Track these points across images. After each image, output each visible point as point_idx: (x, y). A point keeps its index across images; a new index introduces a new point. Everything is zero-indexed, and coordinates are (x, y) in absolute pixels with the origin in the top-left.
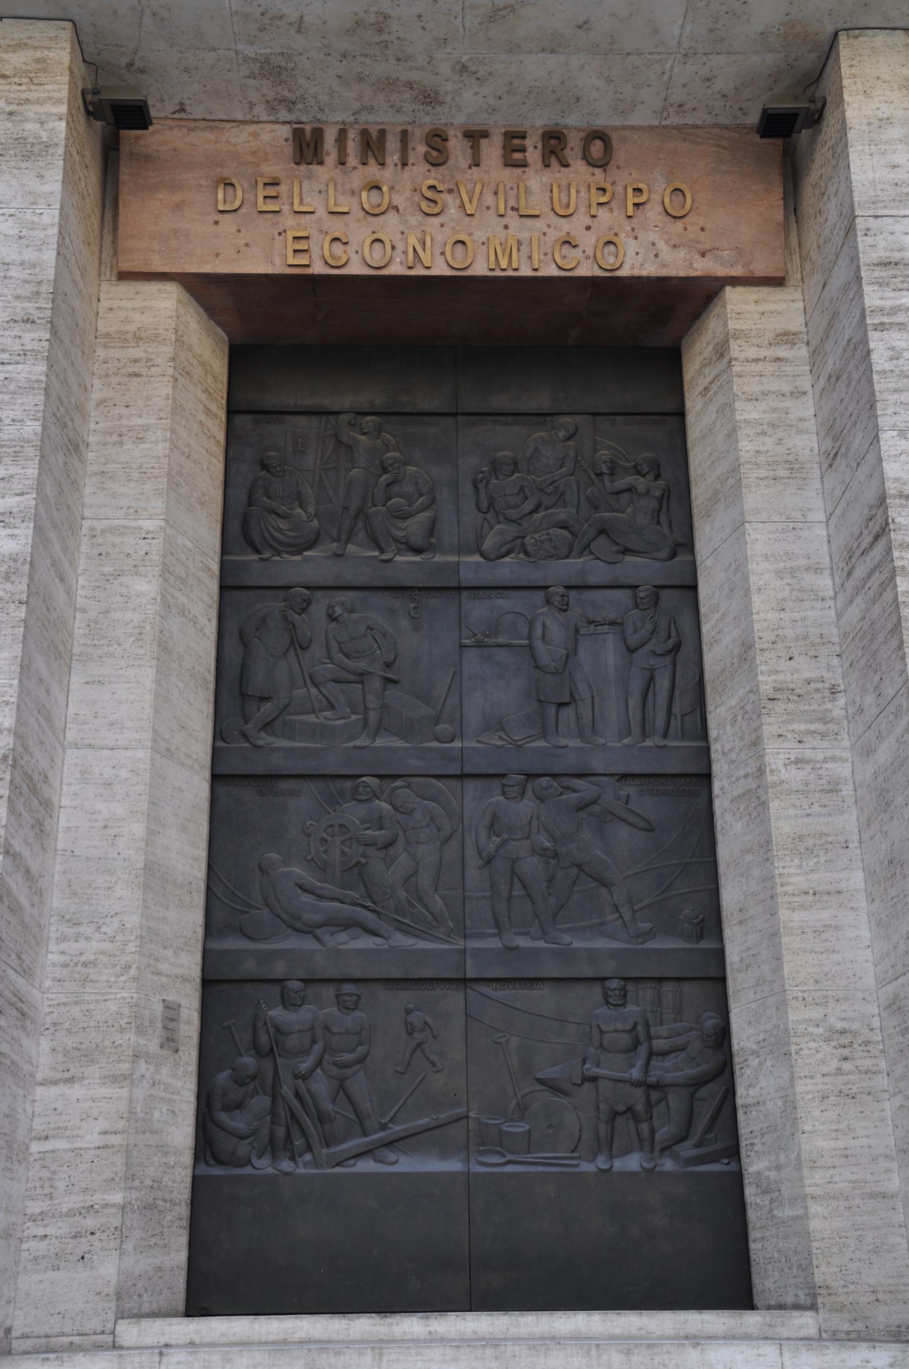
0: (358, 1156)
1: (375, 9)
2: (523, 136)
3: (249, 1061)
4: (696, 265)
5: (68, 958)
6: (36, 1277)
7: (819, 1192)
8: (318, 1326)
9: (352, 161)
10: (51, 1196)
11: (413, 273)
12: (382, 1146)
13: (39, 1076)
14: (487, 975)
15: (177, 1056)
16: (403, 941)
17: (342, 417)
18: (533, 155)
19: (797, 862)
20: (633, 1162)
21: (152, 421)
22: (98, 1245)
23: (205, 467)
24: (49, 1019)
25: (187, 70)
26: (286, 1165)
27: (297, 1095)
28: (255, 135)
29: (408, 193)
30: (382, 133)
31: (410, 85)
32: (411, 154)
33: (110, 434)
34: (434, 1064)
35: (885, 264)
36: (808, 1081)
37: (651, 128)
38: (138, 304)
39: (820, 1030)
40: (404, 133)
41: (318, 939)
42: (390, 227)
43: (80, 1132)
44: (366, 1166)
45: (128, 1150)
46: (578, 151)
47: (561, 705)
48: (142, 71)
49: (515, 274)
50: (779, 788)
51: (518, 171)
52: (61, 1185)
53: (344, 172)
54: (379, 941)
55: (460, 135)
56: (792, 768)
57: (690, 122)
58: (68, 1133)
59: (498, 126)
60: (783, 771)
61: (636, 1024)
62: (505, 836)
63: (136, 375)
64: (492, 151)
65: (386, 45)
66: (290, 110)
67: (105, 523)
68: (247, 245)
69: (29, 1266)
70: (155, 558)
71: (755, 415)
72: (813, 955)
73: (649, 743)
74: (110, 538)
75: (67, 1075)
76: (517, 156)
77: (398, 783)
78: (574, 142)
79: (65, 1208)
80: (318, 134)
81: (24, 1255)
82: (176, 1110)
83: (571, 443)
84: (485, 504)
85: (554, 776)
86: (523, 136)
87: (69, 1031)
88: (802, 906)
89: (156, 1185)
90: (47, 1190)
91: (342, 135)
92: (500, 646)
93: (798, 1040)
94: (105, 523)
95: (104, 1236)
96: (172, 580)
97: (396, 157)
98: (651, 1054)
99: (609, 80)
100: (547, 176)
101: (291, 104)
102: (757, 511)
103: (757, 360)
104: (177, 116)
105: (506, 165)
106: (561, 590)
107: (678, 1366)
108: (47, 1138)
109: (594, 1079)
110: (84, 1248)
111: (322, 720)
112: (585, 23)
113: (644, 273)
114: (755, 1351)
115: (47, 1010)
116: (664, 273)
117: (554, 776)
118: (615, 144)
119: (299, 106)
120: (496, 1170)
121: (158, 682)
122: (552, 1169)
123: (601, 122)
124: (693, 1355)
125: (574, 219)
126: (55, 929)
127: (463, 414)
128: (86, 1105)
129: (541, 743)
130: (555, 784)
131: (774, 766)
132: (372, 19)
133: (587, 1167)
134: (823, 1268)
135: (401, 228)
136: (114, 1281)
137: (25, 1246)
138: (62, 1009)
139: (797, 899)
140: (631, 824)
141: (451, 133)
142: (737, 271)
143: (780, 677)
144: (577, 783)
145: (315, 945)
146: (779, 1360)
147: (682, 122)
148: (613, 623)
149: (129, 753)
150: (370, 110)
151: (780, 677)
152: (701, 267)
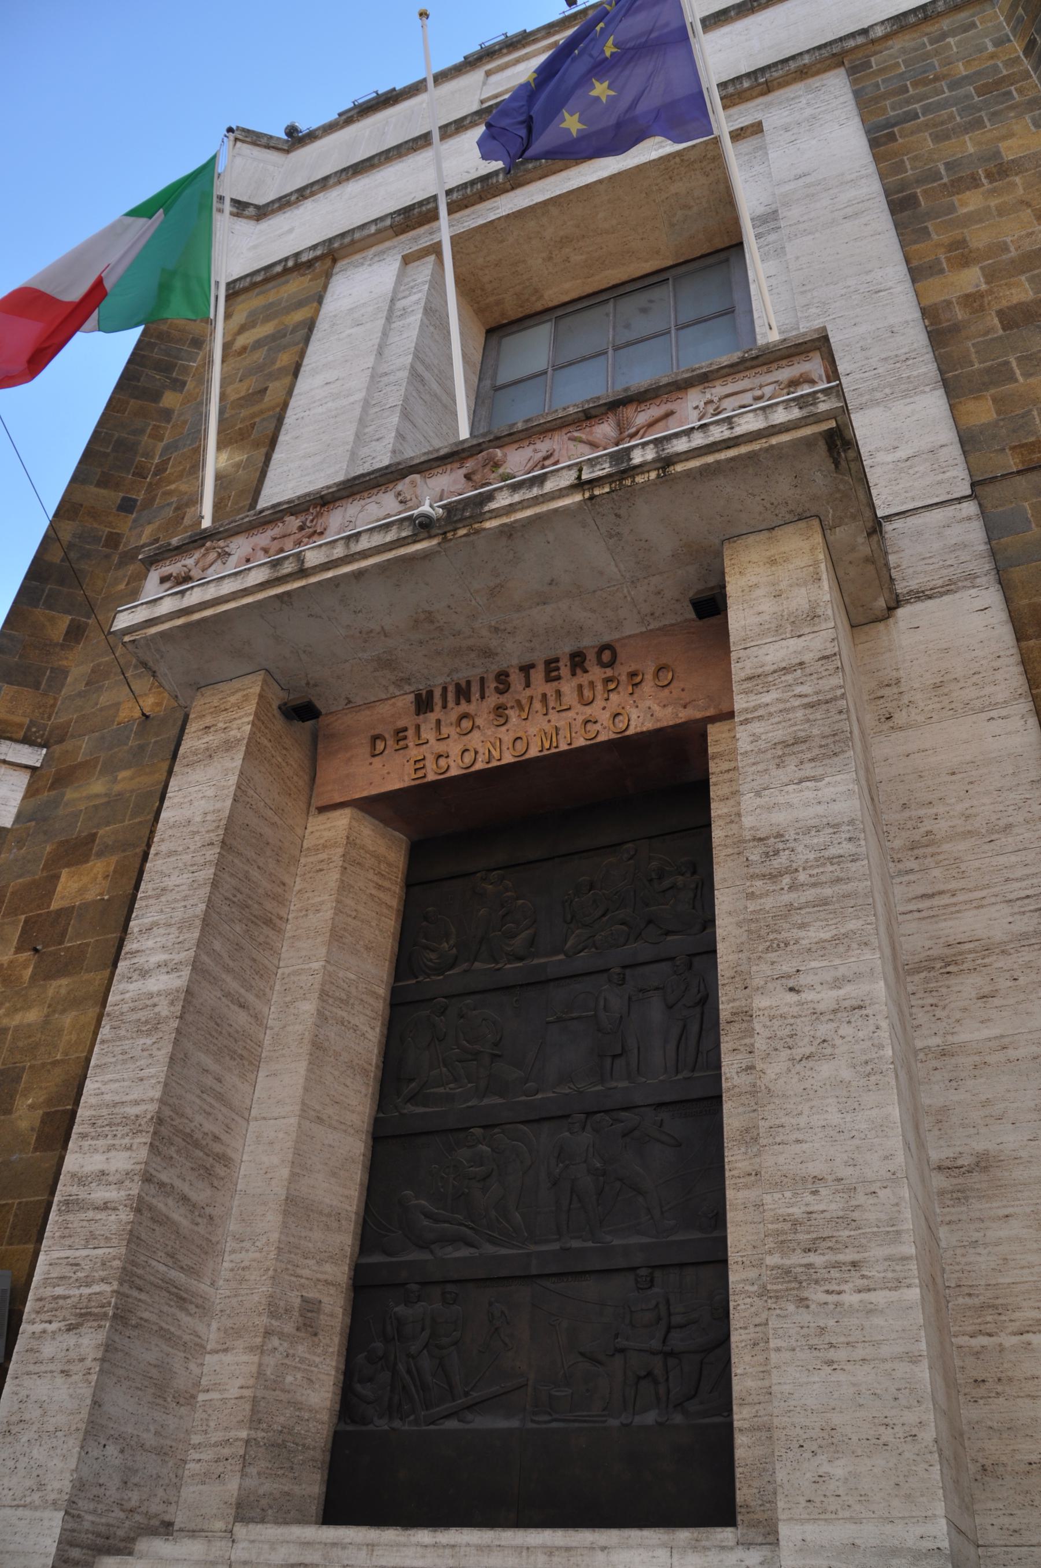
0: (447, 1417)
1: (420, 610)
2: (557, 660)
3: (378, 1345)
4: (680, 715)
5: (234, 1265)
6: (192, 1489)
7: (746, 1425)
8: (360, 1534)
9: (451, 704)
10: (206, 1432)
11: (490, 766)
12: (464, 1409)
13: (209, 1348)
14: (547, 1271)
15: (316, 1339)
16: (490, 1249)
17: (478, 875)
18: (565, 671)
19: (743, 1150)
20: (650, 1418)
21: (326, 897)
22: (229, 1468)
23: (374, 924)
24: (219, 1308)
25: (339, 677)
26: (397, 1424)
27: (409, 1372)
28: (394, 705)
29: (485, 716)
30: (469, 683)
31: (471, 649)
32: (487, 690)
33: (301, 911)
34: (506, 1344)
35: (750, 678)
36: (742, 1331)
37: (642, 633)
38: (329, 825)
39: (755, 1288)
40: (482, 679)
41: (432, 1252)
42: (475, 739)
43: (227, 1387)
44: (452, 1424)
45: (255, 1400)
46: (594, 660)
47: (615, 1057)
48: (316, 685)
49: (557, 750)
50: (732, 1092)
51: (556, 683)
52: (212, 1424)
53: (446, 713)
54: (472, 1250)
55: (517, 671)
56: (743, 1075)
57: (667, 623)
58: (221, 1387)
59: (539, 657)
60: (736, 1077)
61: (657, 1305)
62: (567, 1162)
63: (321, 870)
64: (538, 676)
65: (440, 629)
66: (410, 684)
67: (291, 968)
68: (388, 773)
69: (189, 1481)
70: (317, 986)
71: (726, 810)
72: (753, 1226)
73: (680, 1076)
74: (292, 978)
75: (225, 1346)
76: (554, 674)
77: (496, 1130)
78: (591, 656)
79: (213, 1440)
80: (430, 694)
81: (187, 1472)
82: (314, 1378)
83: (631, 862)
84: (569, 917)
85: (606, 1112)
86: (557, 660)
87: (229, 1316)
88: (746, 1186)
89: (285, 1430)
90: (204, 1428)
91: (445, 689)
92: (573, 1019)
93: (736, 1297)
94: (291, 968)
95: (233, 1462)
96: (331, 1001)
97: (478, 695)
98: (669, 1328)
99: (594, 611)
100: (574, 682)
101: (408, 680)
102: (725, 880)
103: (728, 771)
104: (349, 706)
105: (547, 681)
106: (618, 970)
107: (588, 1565)
108: (208, 1391)
109: (622, 1351)
110: (221, 1469)
111: (448, 1090)
112: (552, 580)
113: (645, 729)
114: (650, 1554)
115: (218, 1301)
116: (659, 725)
117: (606, 1112)
118: (618, 650)
119: (413, 680)
120: (544, 1426)
121: (309, 1070)
122: (585, 1425)
123: (606, 639)
124: (601, 1556)
125: (594, 705)
126: (230, 1244)
127: (559, 857)
128: (233, 1368)
129: (600, 1088)
130: (607, 1118)
131: (728, 1075)
132: (423, 616)
133: (614, 1422)
134: (745, 1490)
135: (482, 738)
136: (236, 1494)
137: (187, 1466)
138: (227, 1300)
139: (741, 1180)
140: (663, 1143)
141: (511, 671)
142: (711, 712)
143: (737, 1004)
144: (624, 1115)
145: (429, 1257)
146: (669, 1561)
147: (661, 624)
148: (657, 989)
149: (285, 1121)
150: (457, 670)
151: (737, 1004)
152: (684, 715)
